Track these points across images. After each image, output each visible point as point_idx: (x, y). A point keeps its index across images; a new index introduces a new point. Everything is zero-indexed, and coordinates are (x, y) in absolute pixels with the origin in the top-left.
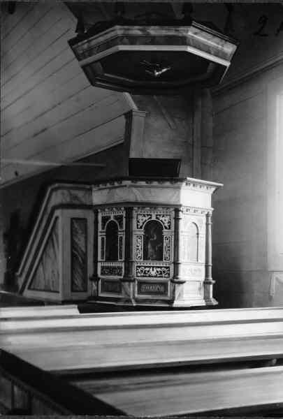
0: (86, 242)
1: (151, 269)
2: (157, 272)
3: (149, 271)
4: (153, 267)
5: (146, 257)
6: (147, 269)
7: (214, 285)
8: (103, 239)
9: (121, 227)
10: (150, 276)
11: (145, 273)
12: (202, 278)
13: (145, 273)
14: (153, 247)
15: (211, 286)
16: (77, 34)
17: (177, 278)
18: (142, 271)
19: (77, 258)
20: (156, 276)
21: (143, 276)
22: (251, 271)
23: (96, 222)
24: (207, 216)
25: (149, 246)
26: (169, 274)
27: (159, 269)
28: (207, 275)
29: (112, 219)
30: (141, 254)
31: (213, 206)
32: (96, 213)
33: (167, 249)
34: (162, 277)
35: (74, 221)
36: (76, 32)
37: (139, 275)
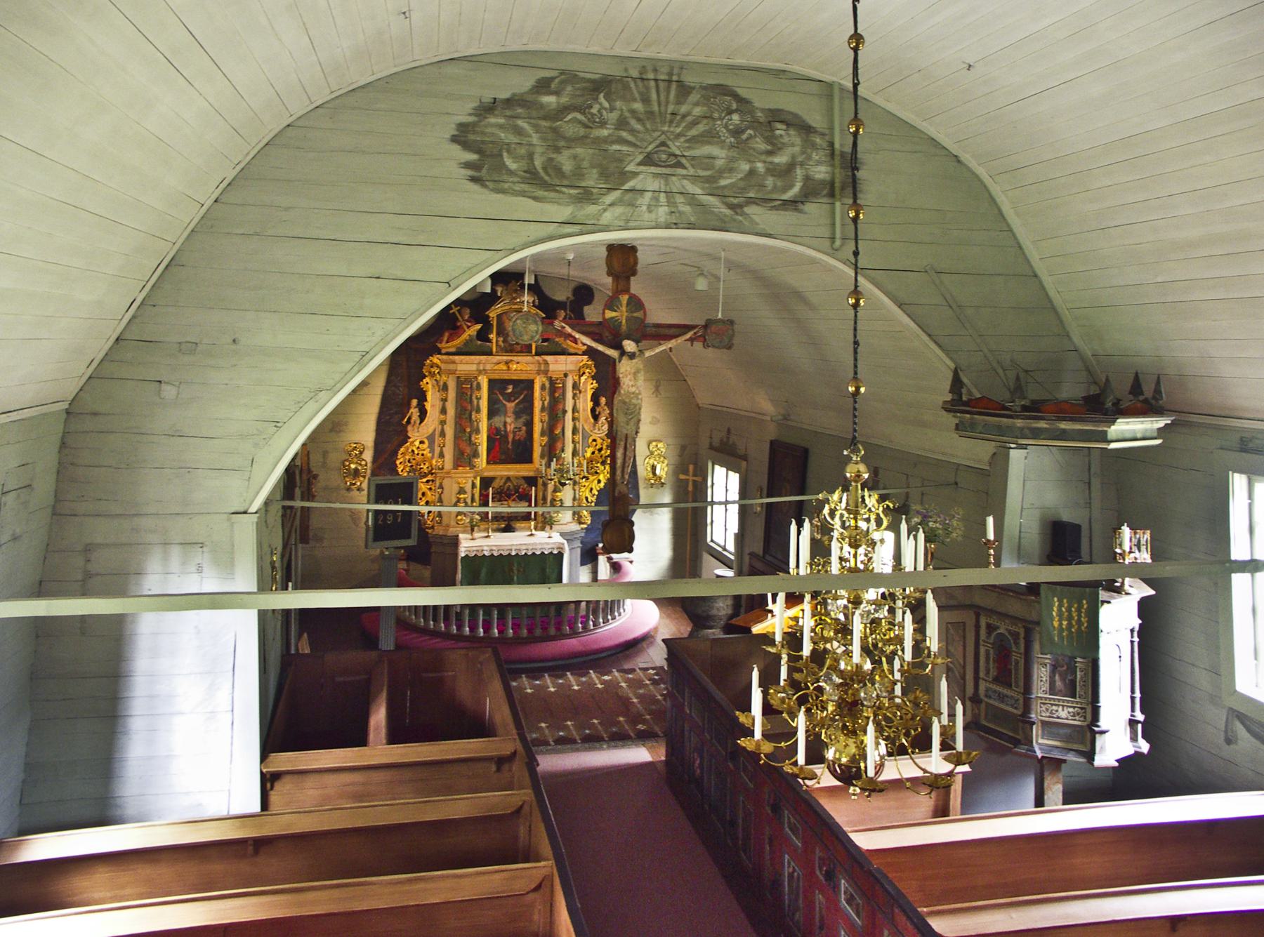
0: (964, 647)
1: (1061, 708)
2: (1069, 713)
3: (1057, 711)
4: (1063, 706)
5: (1052, 690)
6: (1054, 708)
7: (1143, 724)
8: (987, 653)
9: (1016, 644)
10: (1058, 718)
11: (1051, 713)
12: (1127, 715)
13: (1051, 713)
14: (1063, 679)
15: (1140, 726)
16: (1116, 764)
17: (1098, 726)
18: (1047, 710)
19: (953, 671)
20: (1067, 719)
21: (1050, 717)
22: (1186, 683)
23: (977, 627)
24: (1132, 631)
25: (1057, 677)
26: (1085, 717)
27: (1071, 710)
28: (1133, 709)
29: (1001, 631)
30: (1046, 687)
31: (1139, 616)
32: (978, 616)
33: (1082, 683)
34: (1075, 720)
35: (949, 625)
36: (1117, 761)
37: (1044, 714)
